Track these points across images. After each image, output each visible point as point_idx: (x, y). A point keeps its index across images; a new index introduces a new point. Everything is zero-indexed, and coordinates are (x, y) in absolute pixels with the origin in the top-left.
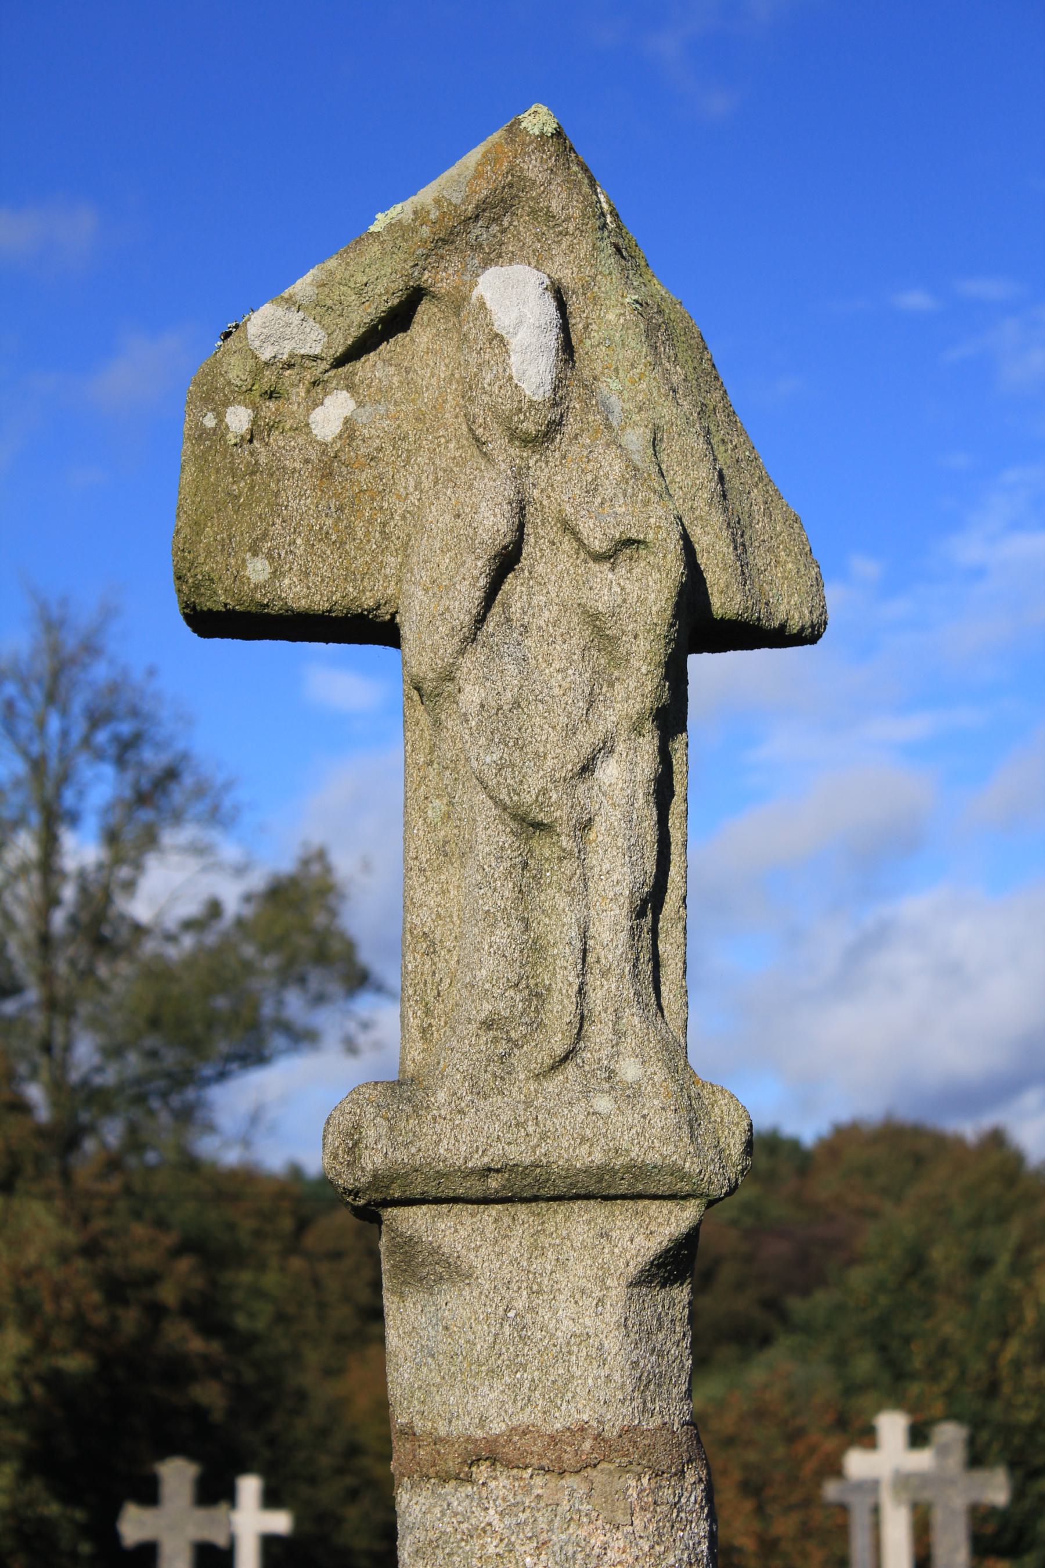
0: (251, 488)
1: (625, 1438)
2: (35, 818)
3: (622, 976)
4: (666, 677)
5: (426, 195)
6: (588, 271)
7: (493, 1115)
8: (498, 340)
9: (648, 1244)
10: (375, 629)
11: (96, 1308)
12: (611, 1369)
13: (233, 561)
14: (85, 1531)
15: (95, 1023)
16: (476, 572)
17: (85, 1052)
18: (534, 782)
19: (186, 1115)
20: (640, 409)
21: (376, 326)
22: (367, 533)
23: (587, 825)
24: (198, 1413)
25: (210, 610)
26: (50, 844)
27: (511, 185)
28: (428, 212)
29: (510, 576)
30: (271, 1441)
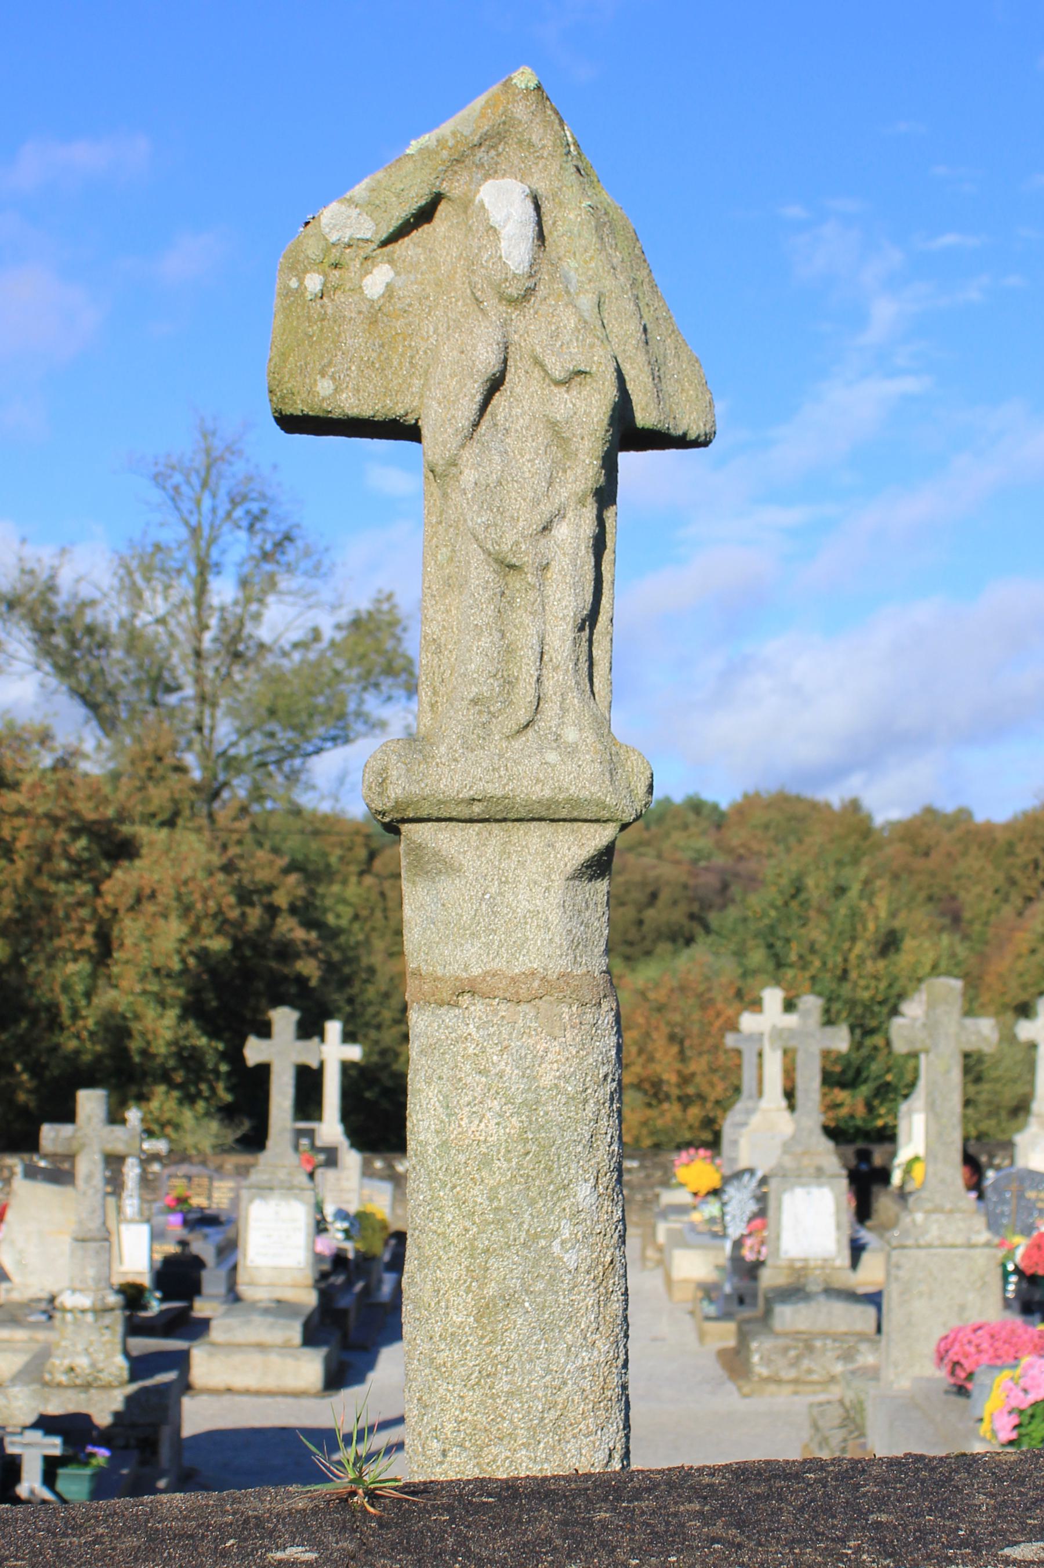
0: (321, 330)
1: (561, 981)
2: (193, 569)
3: (567, 670)
4: (603, 467)
5: (446, 129)
6: (557, 184)
7: (477, 763)
8: (492, 230)
9: (580, 852)
10: (406, 431)
11: (231, 907)
12: (553, 935)
13: (307, 381)
14: (223, 1056)
15: (232, 712)
16: (474, 391)
17: (225, 731)
18: (510, 538)
19: (293, 777)
20: (590, 281)
21: (409, 220)
22: (400, 363)
23: (546, 567)
24: (301, 980)
25: (292, 415)
26: (202, 588)
27: (504, 123)
28: (447, 141)
29: (497, 394)
30: (351, 1001)
